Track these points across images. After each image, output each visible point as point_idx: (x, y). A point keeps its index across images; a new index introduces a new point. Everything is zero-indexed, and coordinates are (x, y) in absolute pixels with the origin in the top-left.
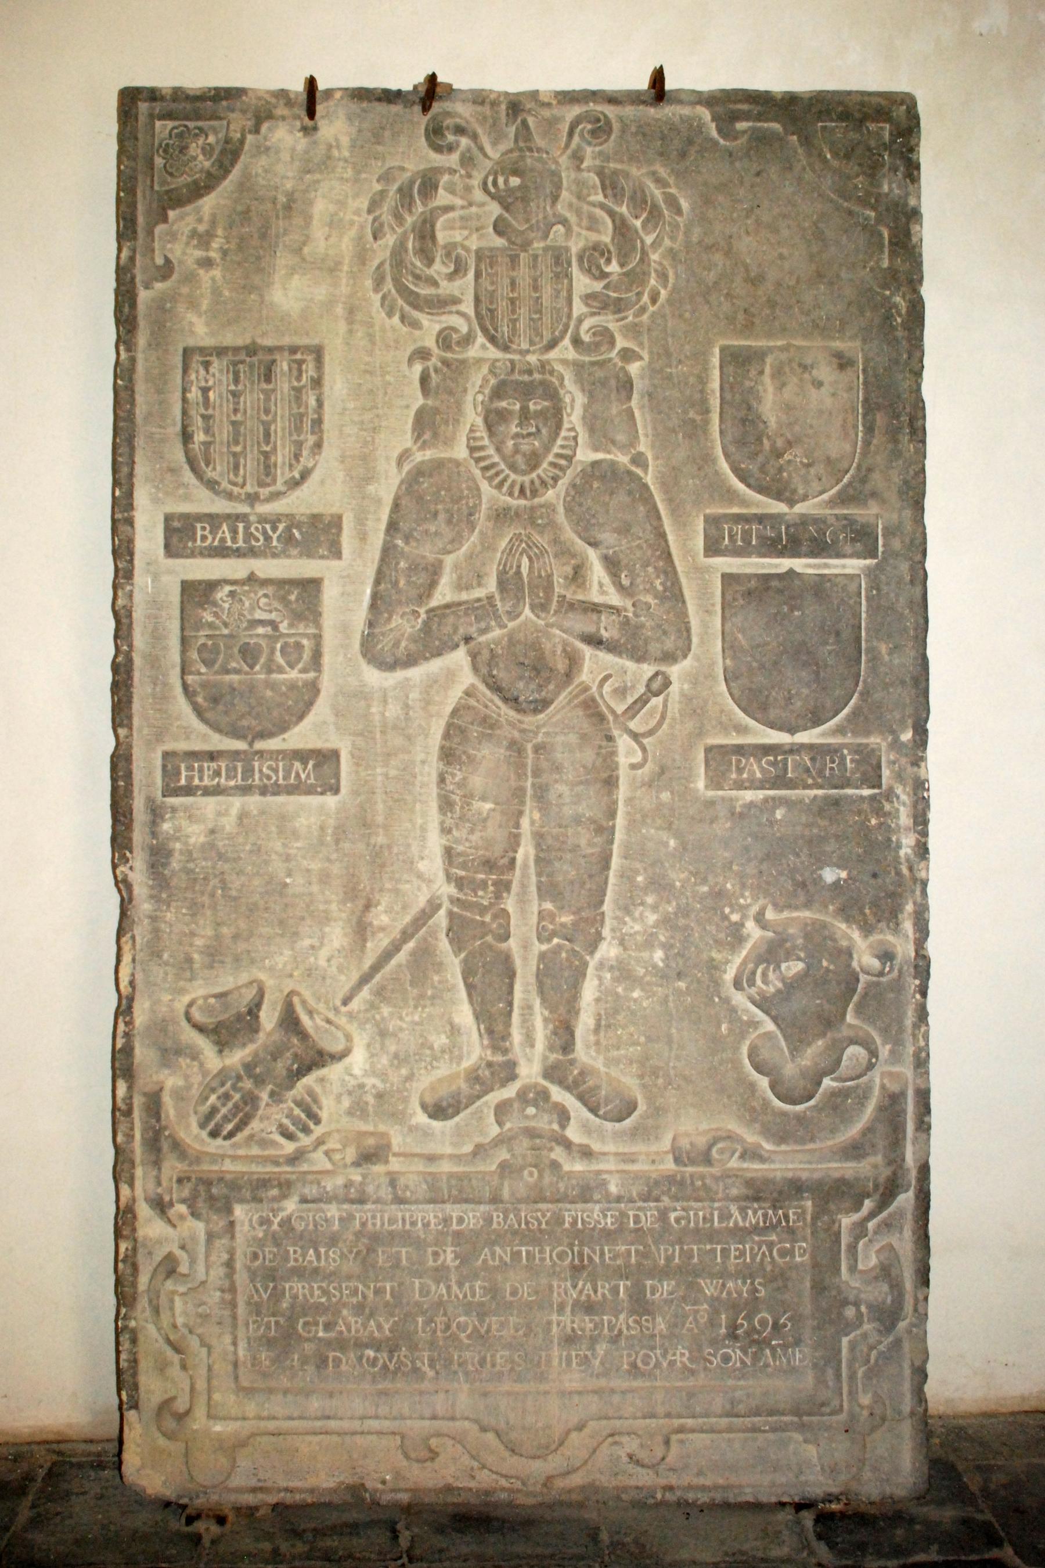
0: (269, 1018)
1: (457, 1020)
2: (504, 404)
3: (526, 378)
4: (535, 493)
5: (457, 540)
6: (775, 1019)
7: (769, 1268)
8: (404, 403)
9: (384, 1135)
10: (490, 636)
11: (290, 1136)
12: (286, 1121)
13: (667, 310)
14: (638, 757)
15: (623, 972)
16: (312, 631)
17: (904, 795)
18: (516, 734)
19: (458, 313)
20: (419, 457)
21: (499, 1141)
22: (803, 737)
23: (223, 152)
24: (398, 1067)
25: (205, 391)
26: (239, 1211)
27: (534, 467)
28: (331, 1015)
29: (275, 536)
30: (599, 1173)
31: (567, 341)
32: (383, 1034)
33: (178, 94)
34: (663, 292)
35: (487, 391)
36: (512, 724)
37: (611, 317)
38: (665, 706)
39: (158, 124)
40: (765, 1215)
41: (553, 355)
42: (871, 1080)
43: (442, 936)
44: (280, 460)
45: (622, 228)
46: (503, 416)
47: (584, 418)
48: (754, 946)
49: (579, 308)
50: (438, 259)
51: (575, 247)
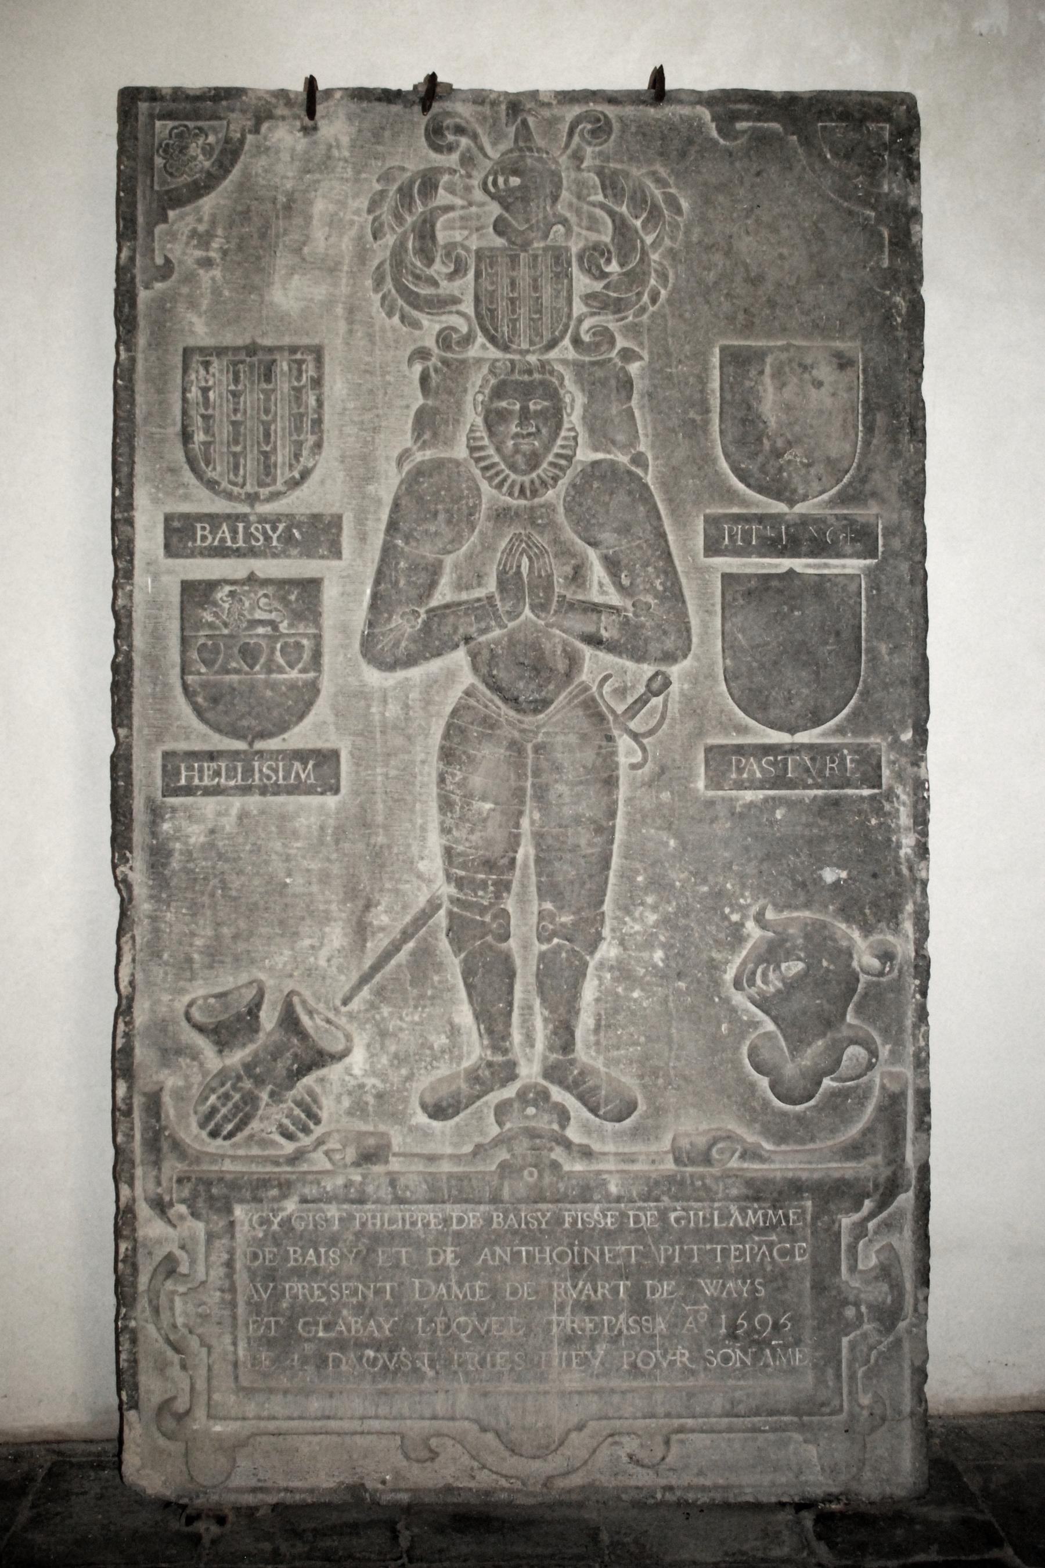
0: (269, 1018)
1: (457, 1020)
2: (504, 404)
3: (526, 378)
4: (535, 493)
5: (457, 540)
6: (775, 1019)
8: (404, 403)
9: (383, 1135)
11: (289, 1137)
12: (286, 1122)
13: (667, 310)
15: (623, 972)
16: (312, 631)
17: (903, 793)
18: (516, 734)
19: (458, 313)
20: (419, 456)
21: (498, 1142)
22: (803, 737)
23: (223, 152)
24: (398, 1067)
25: (205, 391)
26: (239, 1212)
27: (534, 467)
28: (331, 1015)
29: (275, 536)
30: (599, 1173)
31: (567, 342)
32: (383, 1034)
33: (178, 94)
34: (663, 292)
35: (487, 391)
39: (158, 124)
40: (765, 1215)
41: (553, 354)
42: (871, 1081)
43: (442, 936)
44: (280, 460)
45: (621, 227)
46: (503, 416)
47: (584, 418)
48: (754, 947)
49: (579, 308)
50: (438, 260)
51: (575, 249)
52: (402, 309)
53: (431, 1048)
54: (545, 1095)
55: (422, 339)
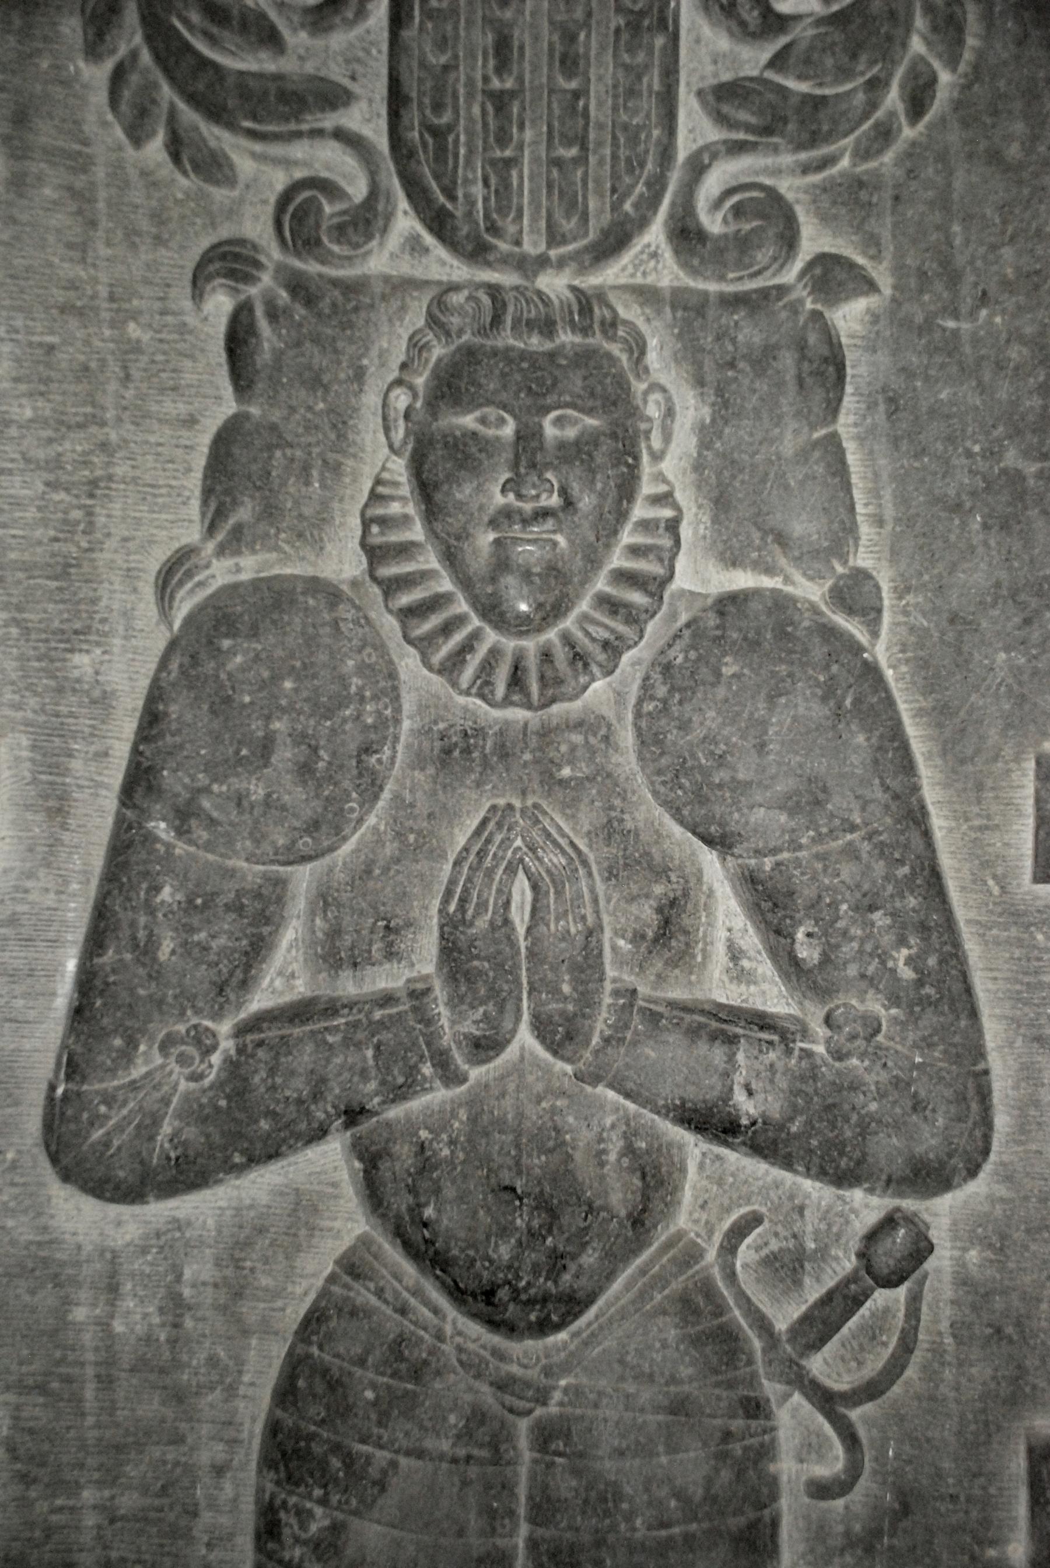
2: (468, 421)
3: (535, 342)
4: (553, 688)
8: (182, 409)
10: (416, 1104)
13: (954, 137)
14: (833, 1463)
18: (486, 1394)
19: (340, 135)
20: (221, 572)
27: (552, 611)
31: (655, 234)
34: (945, 77)
35: (420, 381)
36: (474, 1367)
41: (612, 274)
46: (466, 453)
47: (698, 467)
49: (694, 127)
52: (173, 115)
55: (232, 213)
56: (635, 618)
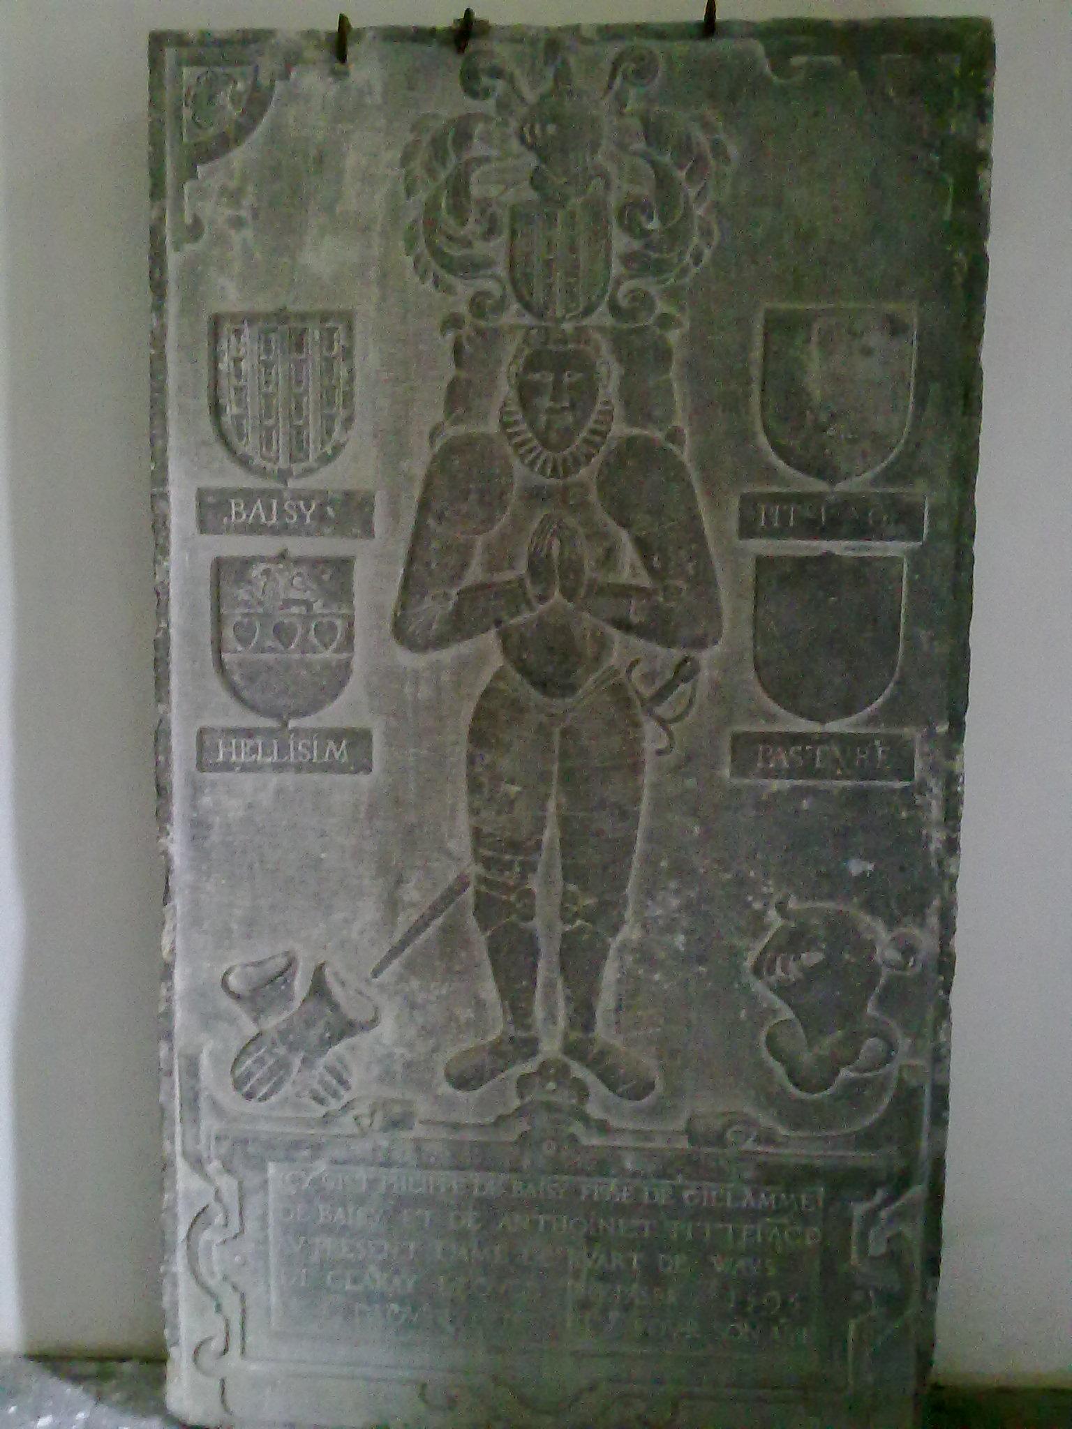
1: (483, 995)
3: (561, 348)
4: (567, 473)
5: (489, 521)
7: (779, 1250)
9: (409, 1103)
11: (321, 1101)
14: (662, 745)
15: (645, 956)
16: (344, 611)
17: (936, 786)
20: (450, 432)
21: (520, 1112)
22: (834, 727)
23: (250, 101)
25: (237, 361)
26: (272, 1169)
30: (614, 1148)
31: (603, 308)
32: (413, 1006)
33: (206, 39)
35: (521, 361)
37: (651, 279)
38: (694, 689)
39: (185, 70)
40: (778, 1199)
41: (585, 322)
43: (470, 914)
45: (663, 181)
48: (775, 935)
49: (616, 269)
50: (471, 219)
51: (613, 201)
53: (457, 1020)
54: (564, 1070)
56: (597, 446)
